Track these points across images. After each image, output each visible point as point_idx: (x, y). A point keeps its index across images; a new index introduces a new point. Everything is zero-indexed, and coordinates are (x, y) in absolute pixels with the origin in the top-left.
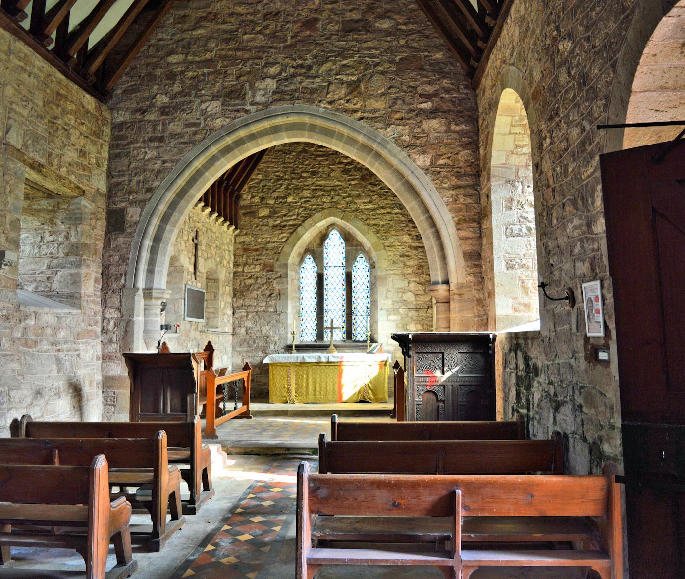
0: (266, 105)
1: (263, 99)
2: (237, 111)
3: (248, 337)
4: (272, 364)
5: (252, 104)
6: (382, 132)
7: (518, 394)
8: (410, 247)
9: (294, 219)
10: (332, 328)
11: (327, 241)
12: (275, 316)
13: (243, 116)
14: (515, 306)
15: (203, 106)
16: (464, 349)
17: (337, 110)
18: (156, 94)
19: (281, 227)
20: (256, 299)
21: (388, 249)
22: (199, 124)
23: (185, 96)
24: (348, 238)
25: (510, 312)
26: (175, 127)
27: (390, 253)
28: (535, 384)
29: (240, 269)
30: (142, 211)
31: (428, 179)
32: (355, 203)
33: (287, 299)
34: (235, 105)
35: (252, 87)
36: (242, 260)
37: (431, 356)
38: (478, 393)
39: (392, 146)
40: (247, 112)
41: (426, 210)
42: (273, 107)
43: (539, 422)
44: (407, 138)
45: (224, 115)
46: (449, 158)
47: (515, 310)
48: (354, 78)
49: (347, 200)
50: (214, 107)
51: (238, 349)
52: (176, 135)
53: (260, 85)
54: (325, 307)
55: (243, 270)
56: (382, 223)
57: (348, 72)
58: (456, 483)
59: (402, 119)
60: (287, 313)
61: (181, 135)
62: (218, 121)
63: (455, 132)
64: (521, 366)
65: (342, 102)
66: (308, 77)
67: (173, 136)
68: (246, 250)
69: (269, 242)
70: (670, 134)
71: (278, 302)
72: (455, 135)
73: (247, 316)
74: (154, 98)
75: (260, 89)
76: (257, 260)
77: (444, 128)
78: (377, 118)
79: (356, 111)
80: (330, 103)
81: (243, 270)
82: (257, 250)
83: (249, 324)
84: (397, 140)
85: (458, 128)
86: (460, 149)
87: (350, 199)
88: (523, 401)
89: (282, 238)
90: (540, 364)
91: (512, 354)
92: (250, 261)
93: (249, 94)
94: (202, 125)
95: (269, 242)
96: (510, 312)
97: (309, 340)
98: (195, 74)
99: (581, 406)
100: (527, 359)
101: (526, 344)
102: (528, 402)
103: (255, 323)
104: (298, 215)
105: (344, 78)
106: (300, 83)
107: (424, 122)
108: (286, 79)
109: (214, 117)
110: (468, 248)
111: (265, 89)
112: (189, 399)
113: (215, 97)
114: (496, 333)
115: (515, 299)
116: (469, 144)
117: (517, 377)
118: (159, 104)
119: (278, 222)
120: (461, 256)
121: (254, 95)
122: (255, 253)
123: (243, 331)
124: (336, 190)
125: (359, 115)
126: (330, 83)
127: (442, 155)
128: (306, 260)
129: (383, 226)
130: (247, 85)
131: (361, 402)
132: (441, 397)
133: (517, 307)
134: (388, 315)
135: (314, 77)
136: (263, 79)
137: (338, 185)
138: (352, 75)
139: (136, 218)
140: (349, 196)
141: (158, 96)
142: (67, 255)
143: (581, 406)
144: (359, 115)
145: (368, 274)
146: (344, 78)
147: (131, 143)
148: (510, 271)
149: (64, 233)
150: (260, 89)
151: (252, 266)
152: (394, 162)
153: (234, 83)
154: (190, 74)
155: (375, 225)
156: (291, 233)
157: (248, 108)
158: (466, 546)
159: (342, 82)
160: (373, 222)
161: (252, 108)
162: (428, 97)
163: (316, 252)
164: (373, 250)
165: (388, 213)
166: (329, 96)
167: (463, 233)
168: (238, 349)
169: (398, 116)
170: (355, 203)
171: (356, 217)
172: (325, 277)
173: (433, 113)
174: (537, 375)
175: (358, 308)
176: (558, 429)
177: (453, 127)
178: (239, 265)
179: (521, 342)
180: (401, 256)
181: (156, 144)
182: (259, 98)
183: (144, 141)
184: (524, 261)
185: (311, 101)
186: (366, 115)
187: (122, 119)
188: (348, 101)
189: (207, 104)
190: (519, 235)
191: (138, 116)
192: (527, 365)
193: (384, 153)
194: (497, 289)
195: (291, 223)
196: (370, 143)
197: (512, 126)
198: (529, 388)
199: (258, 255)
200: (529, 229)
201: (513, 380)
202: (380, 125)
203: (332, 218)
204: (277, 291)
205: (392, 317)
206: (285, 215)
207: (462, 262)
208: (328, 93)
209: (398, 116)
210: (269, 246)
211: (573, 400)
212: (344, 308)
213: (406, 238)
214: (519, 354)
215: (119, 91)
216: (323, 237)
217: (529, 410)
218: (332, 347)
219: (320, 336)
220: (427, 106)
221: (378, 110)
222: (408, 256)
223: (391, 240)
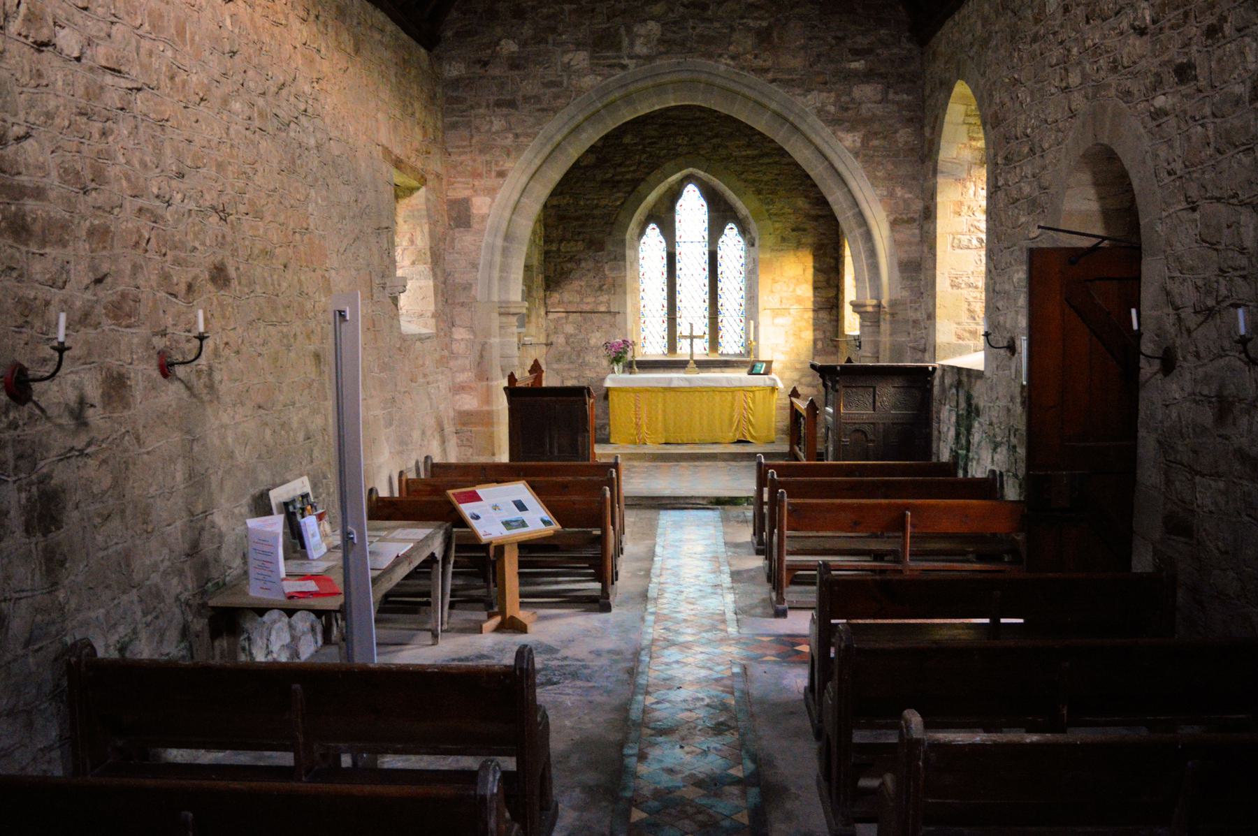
0: (649, 58)
1: (645, 51)
2: (610, 66)
3: (569, 349)
4: (615, 389)
5: (631, 58)
6: (800, 99)
7: (958, 435)
8: (807, 216)
9: (634, 171)
10: (692, 337)
11: (680, 202)
12: (608, 318)
13: (620, 74)
14: (960, 332)
15: (566, 59)
16: (899, 382)
17: (743, 69)
18: (500, 40)
19: (614, 184)
20: (579, 292)
21: (775, 218)
22: (561, 83)
23: (540, 42)
24: (714, 200)
25: (954, 340)
26: (529, 88)
27: (777, 225)
28: (976, 424)
29: (554, 247)
30: (493, 200)
31: (857, 164)
32: (727, 147)
33: (625, 293)
34: (608, 58)
35: (629, 30)
36: (555, 234)
37: (860, 391)
38: (913, 433)
39: (813, 119)
40: (624, 67)
41: (856, 204)
42: (658, 62)
43: (978, 463)
44: (832, 109)
45: (593, 72)
46: (885, 138)
47: (959, 338)
48: (765, 24)
49: (714, 141)
50: (580, 59)
51: (555, 366)
52: (530, 98)
53: (639, 29)
54: (678, 304)
55: (559, 249)
56: (765, 178)
57: (756, 15)
58: (907, 507)
59: (826, 83)
60: (625, 313)
61: (538, 99)
62: (587, 79)
63: (894, 102)
64: (963, 405)
65: (748, 56)
66: (703, 20)
67: (526, 99)
68: (561, 218)
69: (597, 206)
70: (1086, 243)
71: (612, 297)
72: (895, 108)
73: (567, 318)
74: (497, 44)
75: (640, 36)
76: (579, 233)
77: (879, 97)
78: (793, 80)
79: (767, 70)
80: (733, 58)
81: (559, 249)
82: (578, 219)
83: (570, 329)
84: (820, 112)
85: (897, 98)
86: (899, 126)
87: (719, 140)
88: (963, 441)
89: (616, 200)
90: (981, 405)
91: (954, 391)
92: (569, 235)
93: (626, 42)
94: (565, 84)
95: (597, 206)
96: (954, 340)
97: (654, 352)
98: (552, 10)
99: (1014, 447)
100: (969, 398)
101: (970, 382)
102: (968, 442)
103: (579, 328)
104: (640, 163)
105: (751, 23)
106: (694, 28)
107: (855, 89)
108: (675, 23)
109: (581, 74)
110: (904, 256)
111: (647, 36)
112: (580, 439)
113: (579, 46)
114: (936, 365)
115: (959, 324)
116: (910, 120)
117: (958, 416)
118: (505, 52)
119: (609, 175)
120: (896, 265)
121: (632, 44)
122: (575, 223)
123: (561, 340)
124: (696, 126)
125: (770, 76)
126: (732, 29)
127: (876, 134)
128: (648, 231)
129: (766, 183)
130: (622, 31)
131: (739, 442)
132: (871, 437)
133: (961, 332)
134: (774, 317)
135: (711, 21)
136: (645, 20)
137: (699, 118)
138: (762, 19)
139: (485, 210)
140: (716, 136)
141: (503, 43)
142: (413, 263)
143: (1014, 447)
144: (770, 76)
145: (743, 254)
146: (751, 23)
147: (472, 107)
148: (955, 291)
149: (408, 235)
150: (640, 36)
151: (572, 243)
152: (818, 141)
153: (604, 26)
154: (545, 11)
155: (755, 181)
156: (630, 193)
157: (626, 61)
158: (915, 555)
159: (749, 29)
160: (752, 177)
161: (631, 63)
162: (857, 53)
163: (665, 219)
164: (751, 219)
165: (776, 163)
166: (731, 48)
167: (898, 237)
168: (555, 366)
169: (820, 79)
170: (727, 147)
171: (726, 168)
172: (678, 257)
173: (867, 76)
174: (978, 415)
175: (727, 305)
176: (994, 468)
177: (891, 96)
178: (552, 242)
179: (965, 379)
180: (793, 230)
181: (505, 111)
182: (640, 49)
183: (488, 106)
184: (972, 280)
185: (709, 56)
186: (780, 76)
187: (455, 73)
188: (756, 57)
189: (570, 55)
190: (968, 248)
191: (478, 70)
192: (969, 404)
193: (804, 127)
194: (938, 311)
195: (628, 176)
196: (785, 113)
197: (967, 115)
198: (969, 430)
199: (581, 226)
200: (980, 240)
201: (954, 419)
202: (798, 91)
203: (691, 169)
204: (610, 280)
205: (779, 321)
206: (620, 165)
207: (897, 274)
208: (730, 44)
209: (820, 79)
210: (596, 212)
211: (1009, 441)
212: (707, 304)
213: (801, 203)
214: (962, 393)
215: (449, 34)
216: (674, 195)
217: (968, 451)
218: (692, 364)
219: (672, 346)
220: (858, 65)
221: (795, 69)
222: (804, 230)
223: (779, 205)
